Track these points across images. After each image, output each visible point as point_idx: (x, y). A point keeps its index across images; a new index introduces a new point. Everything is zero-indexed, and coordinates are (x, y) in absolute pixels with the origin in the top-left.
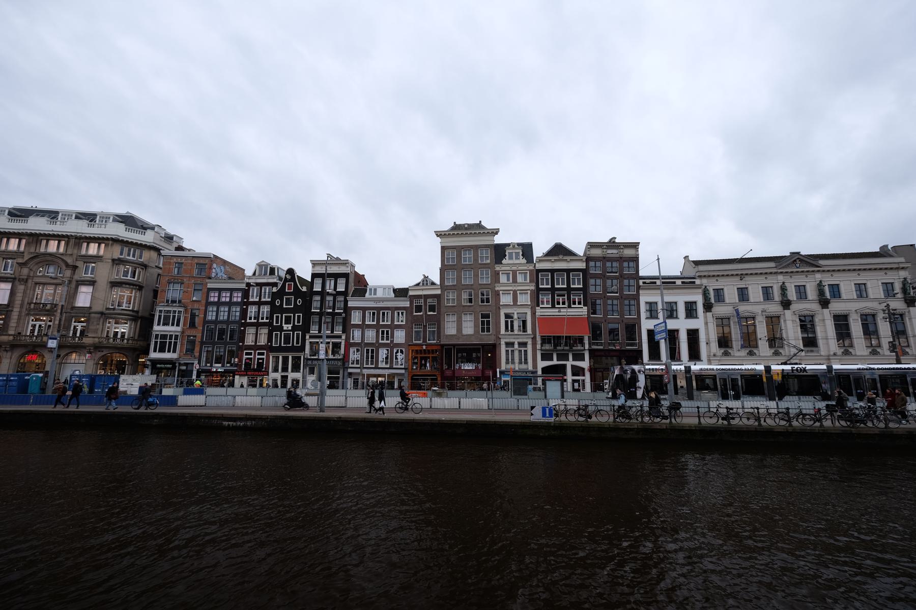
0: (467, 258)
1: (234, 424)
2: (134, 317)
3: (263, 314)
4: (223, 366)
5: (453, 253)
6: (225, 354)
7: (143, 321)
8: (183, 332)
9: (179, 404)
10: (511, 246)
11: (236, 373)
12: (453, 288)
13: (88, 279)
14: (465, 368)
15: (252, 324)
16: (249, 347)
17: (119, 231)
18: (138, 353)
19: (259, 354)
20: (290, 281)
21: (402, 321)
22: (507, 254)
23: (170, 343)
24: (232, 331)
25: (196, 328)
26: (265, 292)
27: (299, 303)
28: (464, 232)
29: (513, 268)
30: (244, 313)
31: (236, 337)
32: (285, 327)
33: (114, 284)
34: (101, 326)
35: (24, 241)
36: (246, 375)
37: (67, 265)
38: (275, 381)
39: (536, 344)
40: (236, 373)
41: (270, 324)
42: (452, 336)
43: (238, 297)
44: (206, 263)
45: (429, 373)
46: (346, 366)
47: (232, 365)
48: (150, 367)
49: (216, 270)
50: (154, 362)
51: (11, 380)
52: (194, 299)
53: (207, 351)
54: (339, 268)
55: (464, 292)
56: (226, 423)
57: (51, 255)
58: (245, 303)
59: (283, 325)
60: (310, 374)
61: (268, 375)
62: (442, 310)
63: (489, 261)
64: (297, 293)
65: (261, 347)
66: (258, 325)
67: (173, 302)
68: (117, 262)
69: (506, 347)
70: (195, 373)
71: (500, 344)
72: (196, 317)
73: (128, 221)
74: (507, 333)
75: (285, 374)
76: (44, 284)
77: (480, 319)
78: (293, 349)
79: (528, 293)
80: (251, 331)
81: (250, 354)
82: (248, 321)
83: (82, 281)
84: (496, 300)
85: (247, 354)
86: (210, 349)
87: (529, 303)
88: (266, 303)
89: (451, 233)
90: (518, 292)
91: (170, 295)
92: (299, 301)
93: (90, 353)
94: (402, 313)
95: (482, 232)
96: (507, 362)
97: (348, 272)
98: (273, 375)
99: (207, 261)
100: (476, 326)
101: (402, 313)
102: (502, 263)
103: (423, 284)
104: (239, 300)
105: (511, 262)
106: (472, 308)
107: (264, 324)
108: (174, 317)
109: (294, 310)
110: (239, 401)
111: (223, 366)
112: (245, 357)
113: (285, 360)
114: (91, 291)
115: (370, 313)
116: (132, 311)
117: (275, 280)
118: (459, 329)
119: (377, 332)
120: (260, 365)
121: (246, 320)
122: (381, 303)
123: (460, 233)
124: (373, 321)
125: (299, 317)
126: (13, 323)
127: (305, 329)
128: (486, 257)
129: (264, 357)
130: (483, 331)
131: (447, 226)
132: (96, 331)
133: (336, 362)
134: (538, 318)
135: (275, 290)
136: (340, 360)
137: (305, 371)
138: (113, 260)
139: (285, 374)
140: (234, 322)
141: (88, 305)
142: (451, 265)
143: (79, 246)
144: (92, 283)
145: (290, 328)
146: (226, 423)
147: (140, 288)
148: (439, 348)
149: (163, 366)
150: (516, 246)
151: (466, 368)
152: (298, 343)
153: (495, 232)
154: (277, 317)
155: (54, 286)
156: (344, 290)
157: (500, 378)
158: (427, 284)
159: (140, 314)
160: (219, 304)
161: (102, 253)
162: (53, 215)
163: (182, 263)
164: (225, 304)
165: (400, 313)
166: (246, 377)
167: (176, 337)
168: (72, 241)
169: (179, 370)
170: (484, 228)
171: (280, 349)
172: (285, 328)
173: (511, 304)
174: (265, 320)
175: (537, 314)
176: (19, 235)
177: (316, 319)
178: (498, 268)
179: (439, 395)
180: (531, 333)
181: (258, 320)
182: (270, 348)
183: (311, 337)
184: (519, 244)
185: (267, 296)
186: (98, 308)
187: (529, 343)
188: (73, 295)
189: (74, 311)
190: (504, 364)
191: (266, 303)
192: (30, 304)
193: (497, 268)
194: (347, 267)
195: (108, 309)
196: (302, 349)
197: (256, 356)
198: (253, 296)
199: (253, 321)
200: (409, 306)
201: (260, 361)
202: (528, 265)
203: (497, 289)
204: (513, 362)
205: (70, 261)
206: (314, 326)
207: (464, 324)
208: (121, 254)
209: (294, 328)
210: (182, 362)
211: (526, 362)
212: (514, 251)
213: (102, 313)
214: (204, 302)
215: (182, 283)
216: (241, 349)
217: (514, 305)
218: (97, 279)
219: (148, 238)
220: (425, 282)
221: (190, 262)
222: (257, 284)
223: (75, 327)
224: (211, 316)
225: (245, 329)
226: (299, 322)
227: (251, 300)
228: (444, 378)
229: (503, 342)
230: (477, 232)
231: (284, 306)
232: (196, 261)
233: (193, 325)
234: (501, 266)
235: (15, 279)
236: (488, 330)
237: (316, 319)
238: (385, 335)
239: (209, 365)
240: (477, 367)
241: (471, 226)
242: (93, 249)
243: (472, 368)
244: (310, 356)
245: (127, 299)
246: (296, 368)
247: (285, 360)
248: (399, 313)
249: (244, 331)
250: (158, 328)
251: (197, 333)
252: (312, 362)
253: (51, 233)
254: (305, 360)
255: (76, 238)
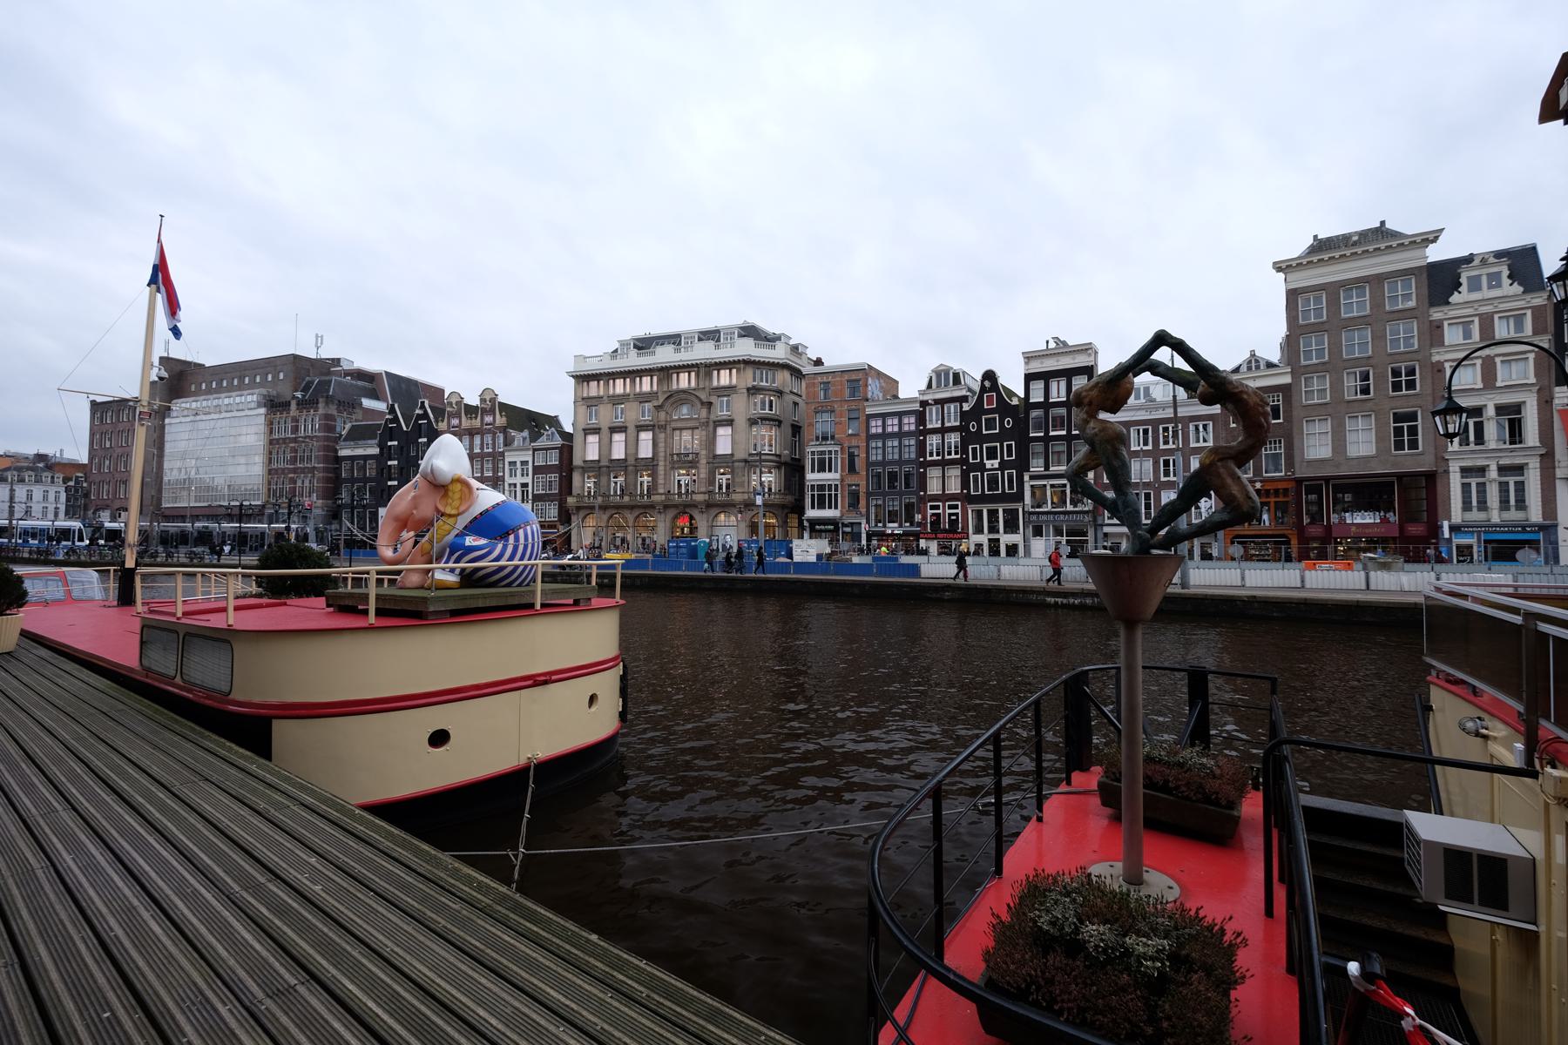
0: (1355, 306)
1: (1065, 601)
2: (779, 463)
3: (950, 447)
4: (901, 526)
5: (1318, 300)
6: (901, 508)
7: (793, 469)
8: (842, 480)
9: (923, 576)
10: (1477, 262)
11: (922, 536)
12: (1320, 368)
13: (725, 417)
14: (1355, 522)
15: (934, 464)
16: (935, 498)
17: (746, 348)
18: (786, 511)
19: (950, 507)
20: (990, 390)
21: (1205, 441)
22: (1463, 280)
23: (830, 495)
24: (908, 476)
25: (858, 473)
26: (949, 413)
27: (973, 427)
28: (1348, 253)
29: (1481, 308)
30: (921, 447)
31: (914, 482)
32: (989, 464)
33: (753, 422)
34: (746, 478)
35: (655, 378)
36: (936, 538)
37: (702, 403)
38: (979, 546)
39: (1554, 468)
40: (922, 536)
41: (963, 462)
42: (1322, 461)
43: (910, 424)
44: (858, 379)
45: (1270, 533)
46: (1100, 522)
47: (912, 525)
48: (808, 529)
49: (874, 388)
50: (814, 522)
51: (681, 547)
52: (850, 432)
53: (876, 506)
54: (1074, 359)
55: (1348, 374)
56: (1051, 600)
57: (684, 391)
58: (923, 432)
59: (985, 461)
60: (1034, 535)
61: (968, 538)
62: (1295, 413)
63: (1412, 304)
64: (1004, 408)
65: (953, 497)
66: (943, 464)
67: (825, 438)
68: (753, 391)
69: (1462, 477)
70: (864, 536)
71: (1447, 472)
72: (856, 458)
73: (750, 331)
74: (1465, 448)
75: (995, 536)
76: (681, 429)
77: (1392, 425)
78: (1003, 498)
79: (1475, 364)
80: (934, 474)
81: (937, 507)
82: (929, 458)
83: (719, 421)
84: (1433, 383)
85: (932, 508)
86: (880, 502)
87: (1532, 380)
88: (952, 429)
89: (1315, 259)
90: (1498, 360)
91: (819, 429)
92: (973, 425)
93: (741, 512)
94: (1205, 427)
95: (1394, 244)
96: (1467, 506)
97: (1090, 364)
98: (975, 539)
99: (860, 375)
100: (1380, 439)
101: (1205, 427)
102: (1448, 303)
103: (1249, 369)
104: (913, 428)
105: (1476, 296)
106: (1369, 405)
107: (953, 462)
108: (830, 459)
109: (1000, 438)
110: (1007, 572)
111: (901, 526)
112: (930, 512)
113: (993, 514)
114: (730, 432)
115: (1139, 430)
116: (775, 455)
117: (964, 393)
118: (1339, 443)
119: (1156, 463)
120: (953, 523)
121: (925, 457)
122: (1161, 411)
123: (1337, 255)
124: (1146, 443)
125: (1009, 447)
126: (661, 481)
127: (1022, 465)
128: (1408, 297)
129: (959, 511)
130: (1399, 445)
131: (1296, 247)
132: (742, 484)
133: (1080, 517)
134: (1559, 411)
135: (966, 407)
136: (1086, 512)
137: (1027, 531)
138: (748, 389)
139: (995, 536)
140: (909, 462)
141: (729, 452)
142: (1314, 324)
143: (709, 375)
144: (729, 422)
145: (996, 466)
146: (1051, 600)
147: (777, 422)
148: (1290, 485)
149: (822, 527)
150: (1492, 260)
151: (1358, 520)
152: (1011, 487)
153: (1431, 238)
154: (974, 450)
155: (690, 431)
156: (1042, 400)
157: (1449, 540)
158: (1258, 367)
159: (783, 459)
160: (884, 436)
161: (734, 381)
162: (674, 339)
163: (829, 383)
164: (892, 435)
165: (1201, 428)
166: (936, 542)
167: (836, 486)
168: (702, 370)
169: (843, 532)
170: (1395, 235)
171: (983, 499)
172: (988, 466)
173: (1477, 387)
174: (953, 456)
175: (1556, 401)
176: (649, 372)
177: (1038, 447)
178: (1437, 314)
179: (1385, 566)
180: (1538, 444)
181: (943, 456)
182: (968, 499)
183: (1032, 478)
184: (1499, 255)
185: (952, 418)
186: (740, 455)
187: (1531, 466)
188: (711, 441)
189: (718, 460)
190: (1460, 511)
191: (952, 429)
192: (672, 455)
193: (1435, 315)
194: (1090, 355)
195: (750, 455)
196: (1019, 497)
197: (945, 511)
198: (931, 420)
199: (935, 458)
200: (1219, 411)
201: (953, 518)
202: (1528, 297)
203: (1435, 358)
204: (1483, 505)
205: (703, 396)
206: (1035, 461)
207: (1350, 437)
208: (754, 380)
209: (1004, 466)
210: (846, 522)
211: (1521, 504)
212: (1485, 271)
213: (746, 461)
214: (863, 435)
215: (832, 411)
216: (923, 500)
217: (1485, 388)
218: (734, 417)
219: (778, 353)
220: (1253, 364)
221: (838, 379)
222: (937, 402)
223: (679, 481)
224: (876, 456)
225: (925, 471)
226: (1010, 455)
227: (929, 426)
228: (1304, 539)
229: (1454, 468)
230: (1383, 246)
231: (984, 432)
232: (846, 377)
233: (852, 469)
234: (1445, 308)
235: (654, 426)
236: (1413, 444)
237: (1038, 447)
238: (1171, 468)
239: (880, 525)
240: (1384, 520)
241: (1365, 236)
242: (725, 378)
243: (1372, 521)
244: (1032, 507)
245: (768, 440)
246: (1011, 526)
247: (993, 514)
248: (1197, 428)
249: (925, 473)
250: (812, 477)
251: (861, 481)
252: (1038, 517)
253: (681, 364)
254: (1027, 515)
255: (706, 366)
